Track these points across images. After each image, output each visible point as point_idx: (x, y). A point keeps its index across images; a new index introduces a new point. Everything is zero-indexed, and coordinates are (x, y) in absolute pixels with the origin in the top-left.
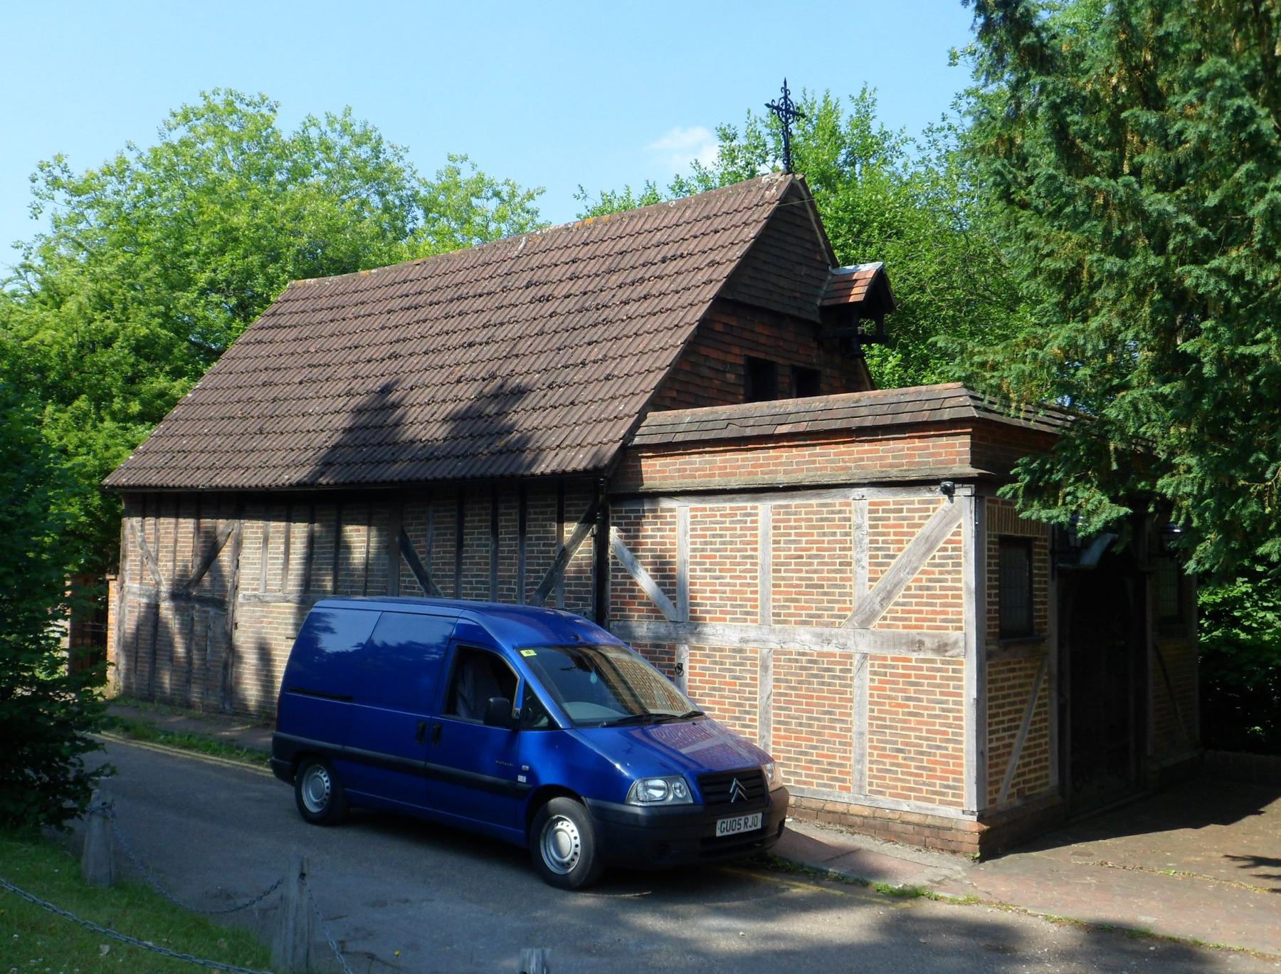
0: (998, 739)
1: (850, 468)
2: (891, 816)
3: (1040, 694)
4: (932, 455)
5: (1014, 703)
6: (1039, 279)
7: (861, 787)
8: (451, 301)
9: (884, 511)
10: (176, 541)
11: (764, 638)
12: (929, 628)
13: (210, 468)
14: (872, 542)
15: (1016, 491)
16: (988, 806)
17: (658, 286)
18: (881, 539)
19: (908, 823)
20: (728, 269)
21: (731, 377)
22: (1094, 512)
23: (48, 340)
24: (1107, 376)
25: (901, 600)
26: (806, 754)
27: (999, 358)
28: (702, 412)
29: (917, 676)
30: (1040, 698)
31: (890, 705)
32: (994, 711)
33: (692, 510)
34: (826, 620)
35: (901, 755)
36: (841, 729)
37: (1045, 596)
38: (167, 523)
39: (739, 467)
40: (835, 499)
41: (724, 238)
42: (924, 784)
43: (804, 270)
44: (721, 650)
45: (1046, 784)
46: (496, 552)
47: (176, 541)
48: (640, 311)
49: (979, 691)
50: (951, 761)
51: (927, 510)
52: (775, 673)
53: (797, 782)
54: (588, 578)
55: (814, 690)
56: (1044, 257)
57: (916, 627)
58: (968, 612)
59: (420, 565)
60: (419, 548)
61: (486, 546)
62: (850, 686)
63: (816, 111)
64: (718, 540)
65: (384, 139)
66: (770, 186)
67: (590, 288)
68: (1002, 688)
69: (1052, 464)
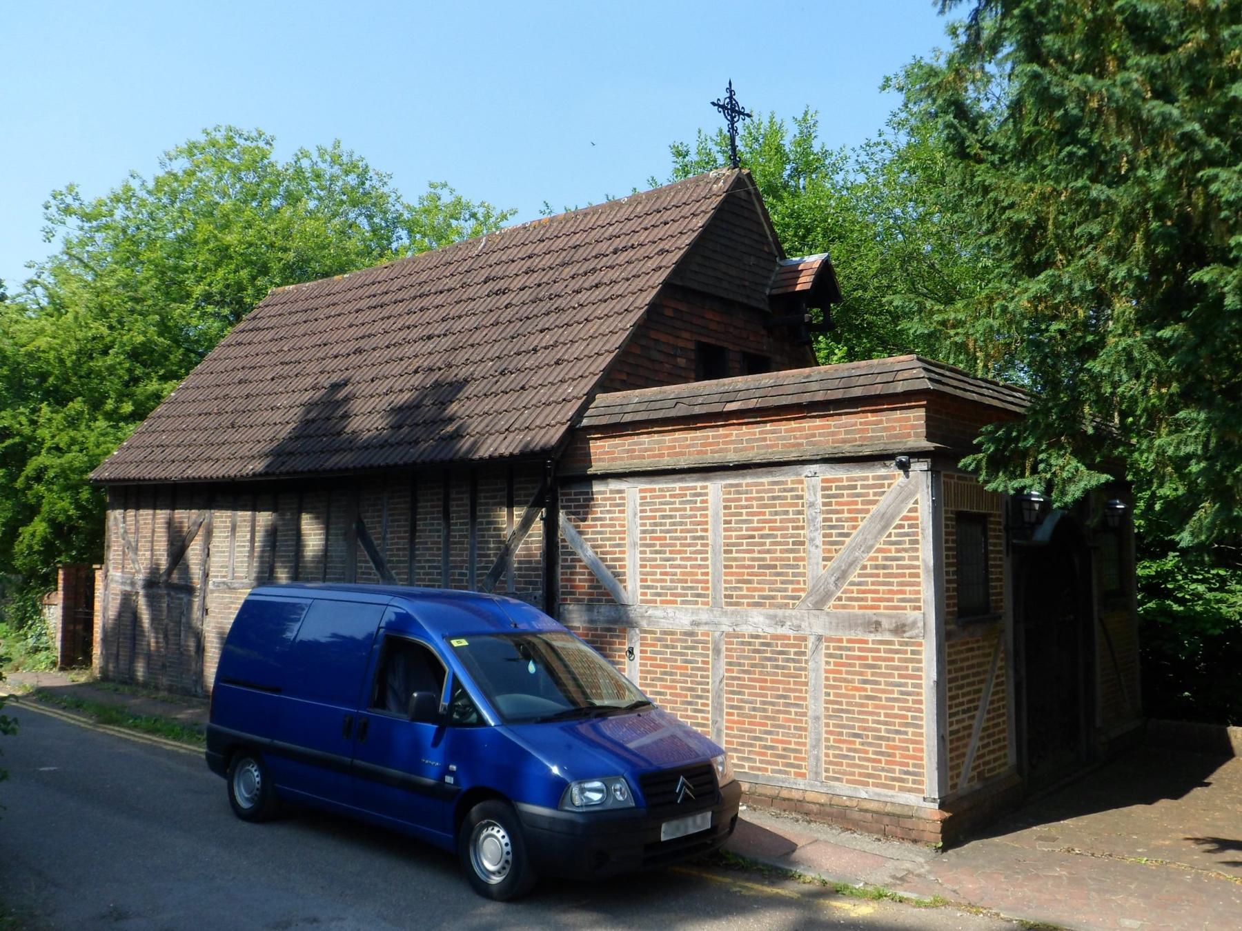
0: (958, 722)
1: (802, 444)
2: (848, 803)
3: (998, 672)
4: (885, 429)
5: (973, 684)
6: (1001, 233)
7: (817, 774)
8: (414, 298)
9: (837, 488)
10: (153, 532)
11: (716, 620)
12: (886, 608)
13: (184, 461)
14: (825, 520)
15: (979, 462)
16: (949, 792)
17: (609, 275)
18: (834, 516)
19: (866, 811)
20: (676, 256)
21: (682, 362)
22: (1070, 480)
23: (44, 346)
24: (1079, 334)
25: (857, 580)
26: (760, 739)
27: (961, 316)
28: (652, 392)
29: (874, 659)
30: (998, 677)
31: (846, 688)
32: (953, 693)
33: (641, 491)
34: (775, 605)
35: (858, 740)
36: (796, 713)
37: (1001, 573)
38: (146, 514)
39: (688, 446)
40: (787, 477)
41: (674, 228)
42: (883, 770)
43: (752, 261)
44: (672, 633)
45: (1005, 764)
46: (448, 536)
47: (153, 532)
48: (592, 299)
49: (939, 673)
50: (911, 746)
51: (882, 486)
52: (727, 656)
53: (751, 768)
54: (538, 562)
55: (768, 674)
56: (1004, 209)
57: (872, 607)
58: (927, 591)
59: (376, 552)
60: (374, 533)
61: (438, 531)
62: (805, 669)
63: (762, 131)
64: (668, 521)
65: (370, 168)
66: (717, 180)
67: (545, 280)
68: (962, 669)
69: (1019, 431)
